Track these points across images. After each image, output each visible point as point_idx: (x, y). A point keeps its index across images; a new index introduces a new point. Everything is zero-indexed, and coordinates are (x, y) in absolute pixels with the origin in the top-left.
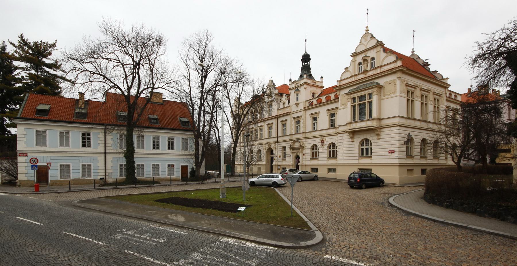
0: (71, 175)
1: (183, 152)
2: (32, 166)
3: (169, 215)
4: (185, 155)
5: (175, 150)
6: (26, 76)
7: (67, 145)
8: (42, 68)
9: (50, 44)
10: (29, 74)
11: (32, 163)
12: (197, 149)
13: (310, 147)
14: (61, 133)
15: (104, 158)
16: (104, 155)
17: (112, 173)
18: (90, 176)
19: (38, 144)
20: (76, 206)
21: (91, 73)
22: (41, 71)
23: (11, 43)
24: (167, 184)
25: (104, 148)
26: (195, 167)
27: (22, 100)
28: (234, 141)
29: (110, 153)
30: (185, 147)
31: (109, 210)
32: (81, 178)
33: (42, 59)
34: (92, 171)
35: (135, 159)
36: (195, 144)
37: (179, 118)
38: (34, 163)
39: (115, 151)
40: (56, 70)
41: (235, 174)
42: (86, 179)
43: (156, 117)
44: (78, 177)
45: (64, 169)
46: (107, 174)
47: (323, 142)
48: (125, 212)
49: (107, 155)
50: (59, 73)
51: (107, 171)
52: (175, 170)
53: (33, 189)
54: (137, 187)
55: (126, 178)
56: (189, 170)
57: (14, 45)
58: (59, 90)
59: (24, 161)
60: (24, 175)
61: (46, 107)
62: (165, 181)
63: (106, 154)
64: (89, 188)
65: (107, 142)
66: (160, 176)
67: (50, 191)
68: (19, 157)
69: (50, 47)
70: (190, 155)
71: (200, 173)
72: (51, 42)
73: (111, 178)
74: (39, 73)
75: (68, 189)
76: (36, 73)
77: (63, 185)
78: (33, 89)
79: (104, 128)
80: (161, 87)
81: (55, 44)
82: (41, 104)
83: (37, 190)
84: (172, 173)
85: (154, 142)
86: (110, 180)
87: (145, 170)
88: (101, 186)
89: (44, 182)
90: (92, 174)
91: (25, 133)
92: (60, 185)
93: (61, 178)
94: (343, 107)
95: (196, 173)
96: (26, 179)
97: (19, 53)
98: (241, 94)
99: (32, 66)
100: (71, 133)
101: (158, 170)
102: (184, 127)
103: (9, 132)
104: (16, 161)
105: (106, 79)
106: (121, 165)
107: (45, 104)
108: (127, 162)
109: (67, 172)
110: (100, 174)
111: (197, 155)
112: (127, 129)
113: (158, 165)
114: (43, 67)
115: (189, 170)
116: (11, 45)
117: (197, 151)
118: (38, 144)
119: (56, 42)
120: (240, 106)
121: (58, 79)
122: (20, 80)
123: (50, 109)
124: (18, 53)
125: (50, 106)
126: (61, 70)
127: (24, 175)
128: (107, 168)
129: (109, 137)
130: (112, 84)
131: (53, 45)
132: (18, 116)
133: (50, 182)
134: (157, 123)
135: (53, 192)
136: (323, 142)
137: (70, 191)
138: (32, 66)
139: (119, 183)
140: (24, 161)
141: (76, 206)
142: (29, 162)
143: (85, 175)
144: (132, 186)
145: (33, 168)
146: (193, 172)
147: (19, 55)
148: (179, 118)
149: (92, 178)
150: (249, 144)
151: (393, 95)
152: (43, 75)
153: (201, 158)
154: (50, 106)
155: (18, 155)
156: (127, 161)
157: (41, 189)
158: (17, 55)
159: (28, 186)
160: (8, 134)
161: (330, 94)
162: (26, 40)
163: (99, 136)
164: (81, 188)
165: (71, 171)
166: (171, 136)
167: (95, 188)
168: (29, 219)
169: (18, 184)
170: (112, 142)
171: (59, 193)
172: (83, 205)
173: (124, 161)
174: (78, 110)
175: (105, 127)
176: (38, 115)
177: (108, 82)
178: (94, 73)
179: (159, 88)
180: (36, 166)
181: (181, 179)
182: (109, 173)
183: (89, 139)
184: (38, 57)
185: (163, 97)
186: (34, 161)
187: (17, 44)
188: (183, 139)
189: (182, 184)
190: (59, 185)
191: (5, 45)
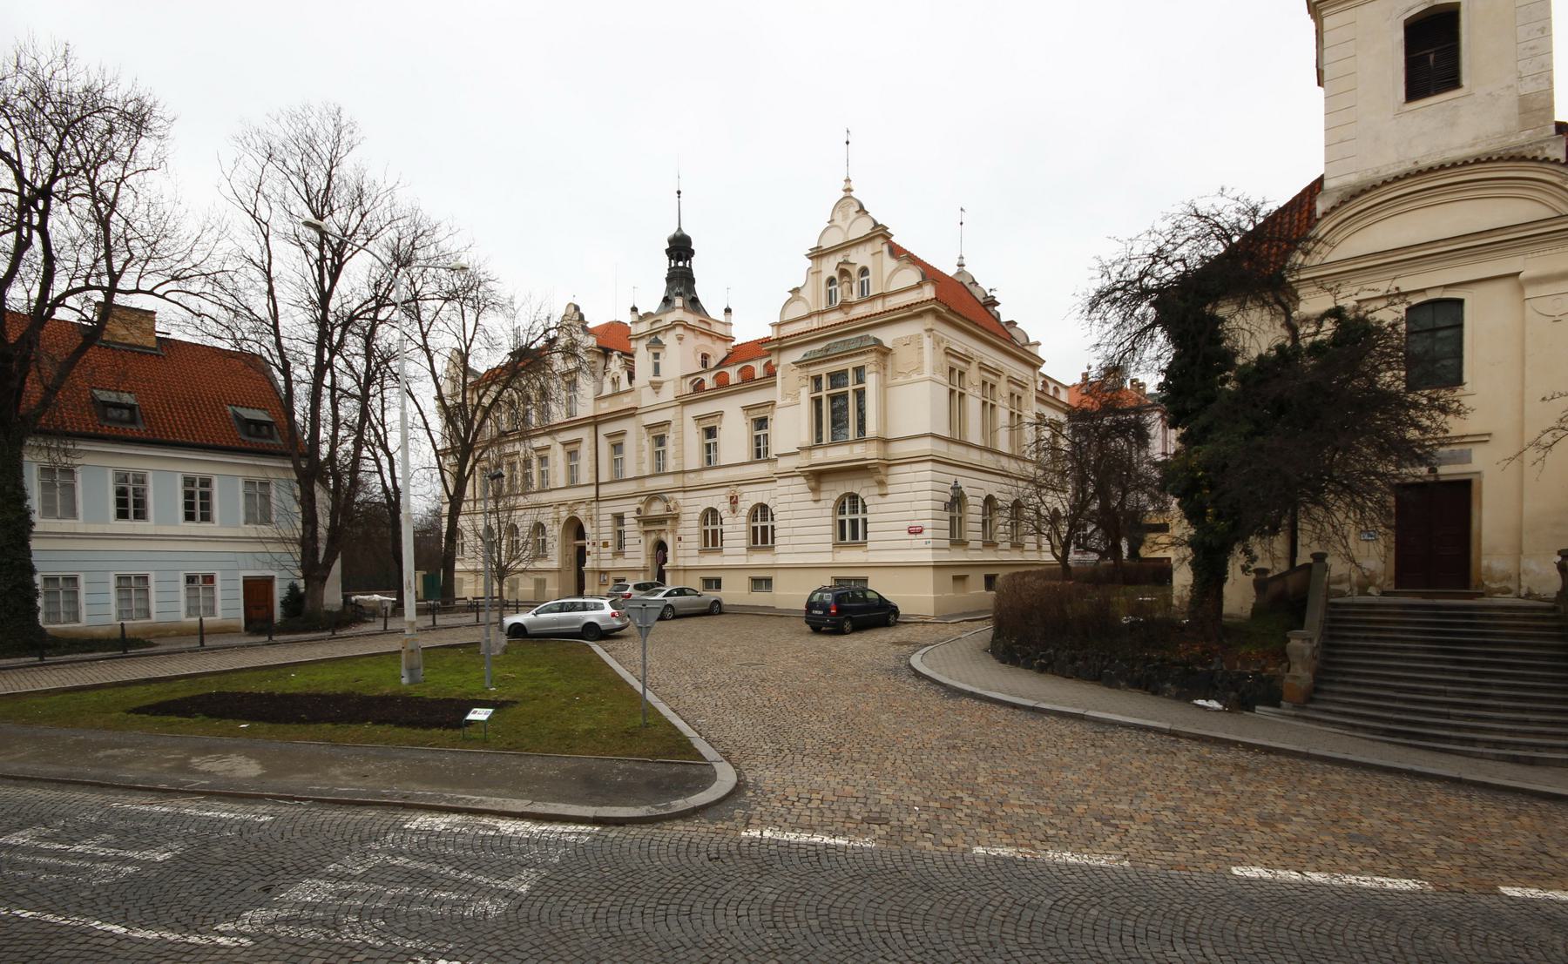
1: (252, 530)
4: (260, 540)
5: (217, 523)
12: (310, 519)
13: (697, 516)
26: (301, 584)
28: (451, 493)
36: (301, 503)
41: (457, 603)
43: (127, 398)
47: (734, 501)
52: (219, 594)
54: (49, 664)
56: (279, 592)
66: (154, 618)
70: (282, 540)
71: (325, 602)
84: (205, 608)
94: (788, 401)
95: (308, 604)
98: (471, 340)
111: (307, 543)
115: (279, 592)
117: (309, 527)
134: (133, 421)
136: (736, 502)
146: (294, 600)
148: (229, 409)
151: (915, 377)
161: (752, 360)
179: (138, 291)
181: (246, 628)
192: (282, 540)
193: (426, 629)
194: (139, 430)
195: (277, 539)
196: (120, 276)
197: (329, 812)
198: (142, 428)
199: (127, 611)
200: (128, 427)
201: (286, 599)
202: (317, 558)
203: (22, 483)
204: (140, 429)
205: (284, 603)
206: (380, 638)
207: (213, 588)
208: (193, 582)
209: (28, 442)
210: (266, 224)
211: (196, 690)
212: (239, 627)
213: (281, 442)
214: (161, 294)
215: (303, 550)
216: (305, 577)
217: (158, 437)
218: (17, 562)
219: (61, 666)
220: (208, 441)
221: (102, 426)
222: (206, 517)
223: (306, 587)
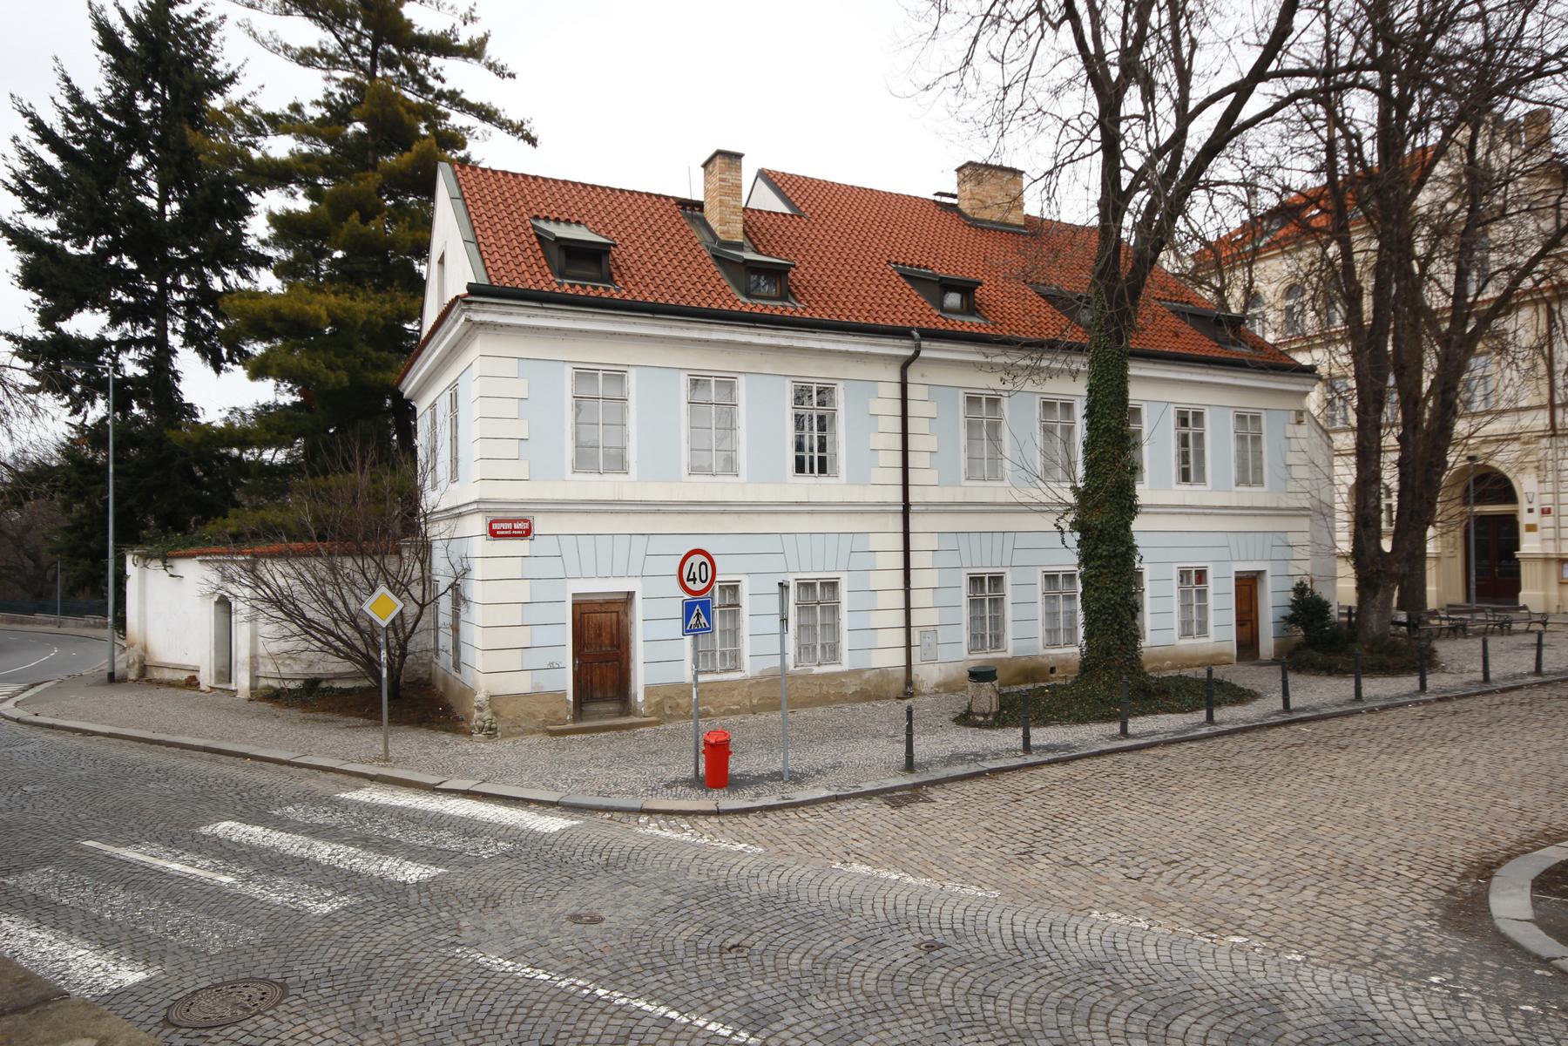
0: (746, 647)
11: (690, 585)
16: (899, 519)
18: (833, 652)
38: (699, 586)
42: (816, 670)
59: (514, 568)
60: (513, 660)
73: (934, 661)
87: (1009, 611)
89: (604, 700)
91: (520, 388)
96: (520, 684)
100: (742, 385)
106: (1051, 578)
126: (491, 66)
127: (513, 660)
133: (640, 697)
140: (514, 568)
145: (693, 621)
149: (846, 664)
150: (387, 480)
159: (533, 732)
163: (877, 406)
182: (925, 630)
186: (695, 569)
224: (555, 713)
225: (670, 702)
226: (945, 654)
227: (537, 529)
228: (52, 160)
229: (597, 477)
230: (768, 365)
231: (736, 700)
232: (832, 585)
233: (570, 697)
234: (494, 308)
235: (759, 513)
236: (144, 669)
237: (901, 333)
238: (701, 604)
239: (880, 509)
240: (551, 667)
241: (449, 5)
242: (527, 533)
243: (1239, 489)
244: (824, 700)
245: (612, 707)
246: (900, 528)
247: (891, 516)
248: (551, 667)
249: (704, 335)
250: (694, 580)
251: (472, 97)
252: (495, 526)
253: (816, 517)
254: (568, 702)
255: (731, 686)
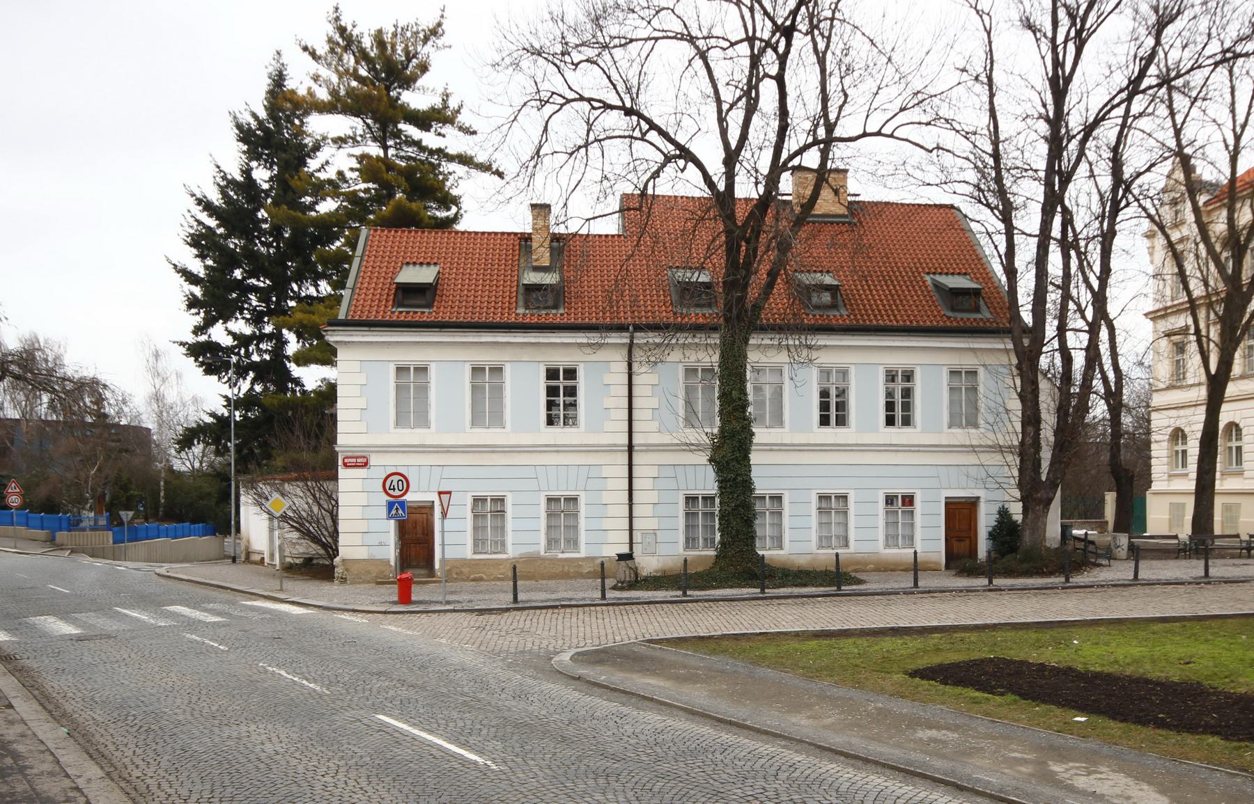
0: (510, 538)
1: (960, 436)
2: (390, 506)
3: (1050, 763)
4: (973, 449)
5: (919, 429)
6: (352, 169)
7: (497, 419)
8: (400, 131)
9: (423, 30)
10: (362, 158)
11: (391, 492)
12: (1031, 419)
14: (477, 370)
15: (624, 471)
17: (654, 532)
18: (573, 543)
19: (401, 420)
20: (574, 678)
21: (594, 108)
22: (396, 143)
23: (305, 49)
24: (896, 586)
25: (625, 426)
26: (1016, 510)
27: (340, 260)
28: (1213, 371)
29: (650, 448)
30: (965, 414)
31: (725, 708)
32: (542, 553)
33: (399, 94)
34: (583, 524)
35: (755, 473)
36: (1022, 397)
37: (928, 278)
38: (397, 493)
39: (666, 439)
40: (443, 131)
41: (1218, 543)
42: (561, 556)
43: (828, 280)
44: (531, 549)
45: (484, 516)
46: (637, 537)
48: (801, 723)
49: (637, 458)
50: (452, 141)
51: (637, 524)
52: (918, 519)
53: (393, 592)
54: (772, 598)
55: (717, 556)
56: (986, 520)
57: (314, 55)
58: (454, 209)
61: (425, 275)
62: (874, 570)
63: (635, 455)
64: (581, 595)
65: (637, 403)
66: (853, 547)
67: (448, 603)
68: (342, 472)
69: (426, 40)
70: (1000, 449)
71: (1048, 534)
72: (428, 22)
74: (391, 152)
75: (510, 597)
76: (381, 153)
77: (481, 579)
78: (372, 217)
79: (628, 341)
80: (875, 130)
81: (439, 25)
82: (408, 264)
83: (405, 598)
84: (904, 537)
85: (824, 394)
86: (648, 563)
88: (622, 589)
90: (583, 537)
92: (474, 580)
93: (475, 553)
95: (1027, 538)
97: (328, 82)
98: (1244, 127)
99: (368, 126)
101: (841, 519)
102: (959, 315)
103: (297, 382)
104: (327, 485)
105: (645, 126)
106: (691, 500)
107: (421, 264)
108: (720, 488)
109: (494, 528)
110: (612, 537)
111: (1028, 451)
112: (723, 338)
113: (844, 498)
114: (401, 126)
115: (986, 520)
116: (306, 54)
117: (1030, 429)
118: (401, 420)
119: (442, 16)
120: (1202, 199)
121: (447, 167)
122: (332, 188)
123: (437, 279)
124: (325, 81)
125: (437, 269)
126: (461, 129)
128: (637, 511)
129: (644, 378)
130: (671, 147)
131: (434, 32)
132: (342, 316)
134: (834, 306)
135: (458, 607)
137: (516, 606)
138: (368, 126)
139: (699, 575)
141: (574, 678)
142: (382, 490)
143: (557, 541)
144: (745, 591)
145: (394, 512)
146: (1005, 530)
147: (331, 94)
148: (928, 278)
149: (583, 553)
152: (402, 158)
153: (1052, 464)
154: (437, 269)
155: (340, 462)
156: (723, 483)
157: (417, 593)
158: (323, 94)
159: (369, 582)
160: (294, 391)
162: (349, 28)
163: (608, 379)
164: (554, 596)
165: (510, 524)
166: (900, 361)
167: (603, 597)
168: (430, 732)
169: (338, 571)
170: (654, 403)
171: (481, 612)
172: (602, 674)
173: (707, 482)
174: (532, 278)
175: (632, 338)
176: (400, 306)
177: (653, 136)
178: (607, 107)
179: (865, 135)
180: (402, 504)
181: (948, 567)
182: (645, 533)
183: (571, 392)
184: (388, 89)
185: (852, 186)
186: (395, 483)
187: (322, 49)
188: (954, 373)
189: (969, 590)
190: (468, 579)
191: (283, 64)
192: (1000, 449)
193: (1196, 582)
194: (841, 316)
195: (990, 446)
196: (836, 123)
197: (864, 775)
198: (844, 313)
199: (826, 537)
200: (832, 313)
201: (995, 528)
202: (1039, 474)
203: (1106, 310)
204: (841, 315)
205: (992, 536)
206: (1127, 592)
207: (912, 512)
208: (892, 504)
209: (751, 342)
210: (988, 14)
211: (982, 652)
212: (940, 564)
213: (988, 315)
214: (889, 133)
215: (1022, 461)
216: (1023, 499)
217: (861, 322)
218: (740, 479)
219: (783, 601)
220: (911, 322)
221: (808, 315)
222: (907, 422)
223: (1025, 511)
224: (383, 572)
225: (455, 571)
226: (664, 550)
227: (372, 462)
228: (212, 223)
229: (409, 430)
230: (526, 355)
231: (501, 571)
232: (573, 500)
233: (392, 563)
234: (341, 333)
235: (519, 452)
236: (248, 554)
237: (621, 328)
238: (399, 503)
239: (611, 449)
240: (381, 545)
241: (431, 89)
242: (365, 465)
243: (950, 430)
244: (565, 576)
245: (423, 572)
246: (626, 462)
247: (620, 454)
248: (381, 545)
249: (476, 340)
250: (394, 489)
251: (452, 151)
252: (346, 461)
253: (561, 454)
254: (391, 566)
255: (498, 563)
